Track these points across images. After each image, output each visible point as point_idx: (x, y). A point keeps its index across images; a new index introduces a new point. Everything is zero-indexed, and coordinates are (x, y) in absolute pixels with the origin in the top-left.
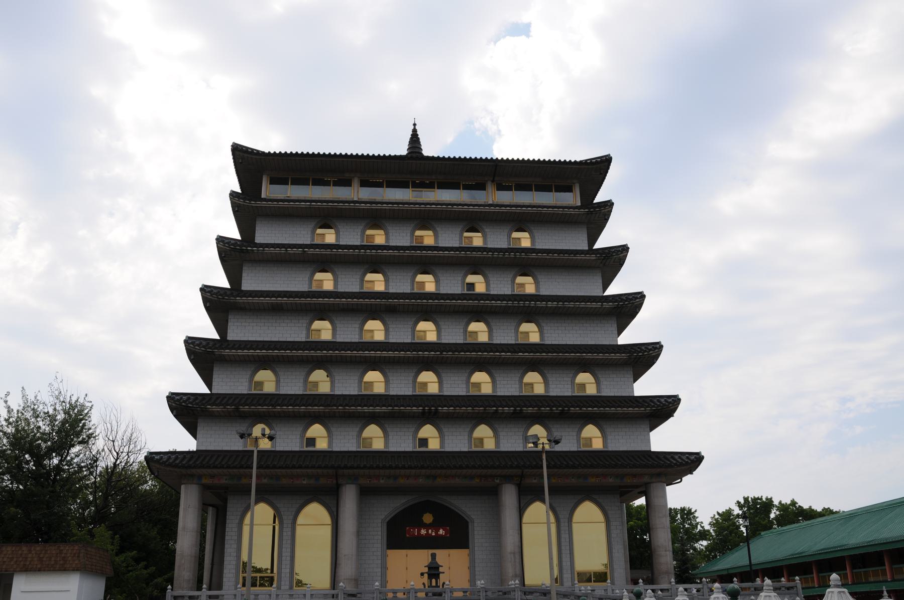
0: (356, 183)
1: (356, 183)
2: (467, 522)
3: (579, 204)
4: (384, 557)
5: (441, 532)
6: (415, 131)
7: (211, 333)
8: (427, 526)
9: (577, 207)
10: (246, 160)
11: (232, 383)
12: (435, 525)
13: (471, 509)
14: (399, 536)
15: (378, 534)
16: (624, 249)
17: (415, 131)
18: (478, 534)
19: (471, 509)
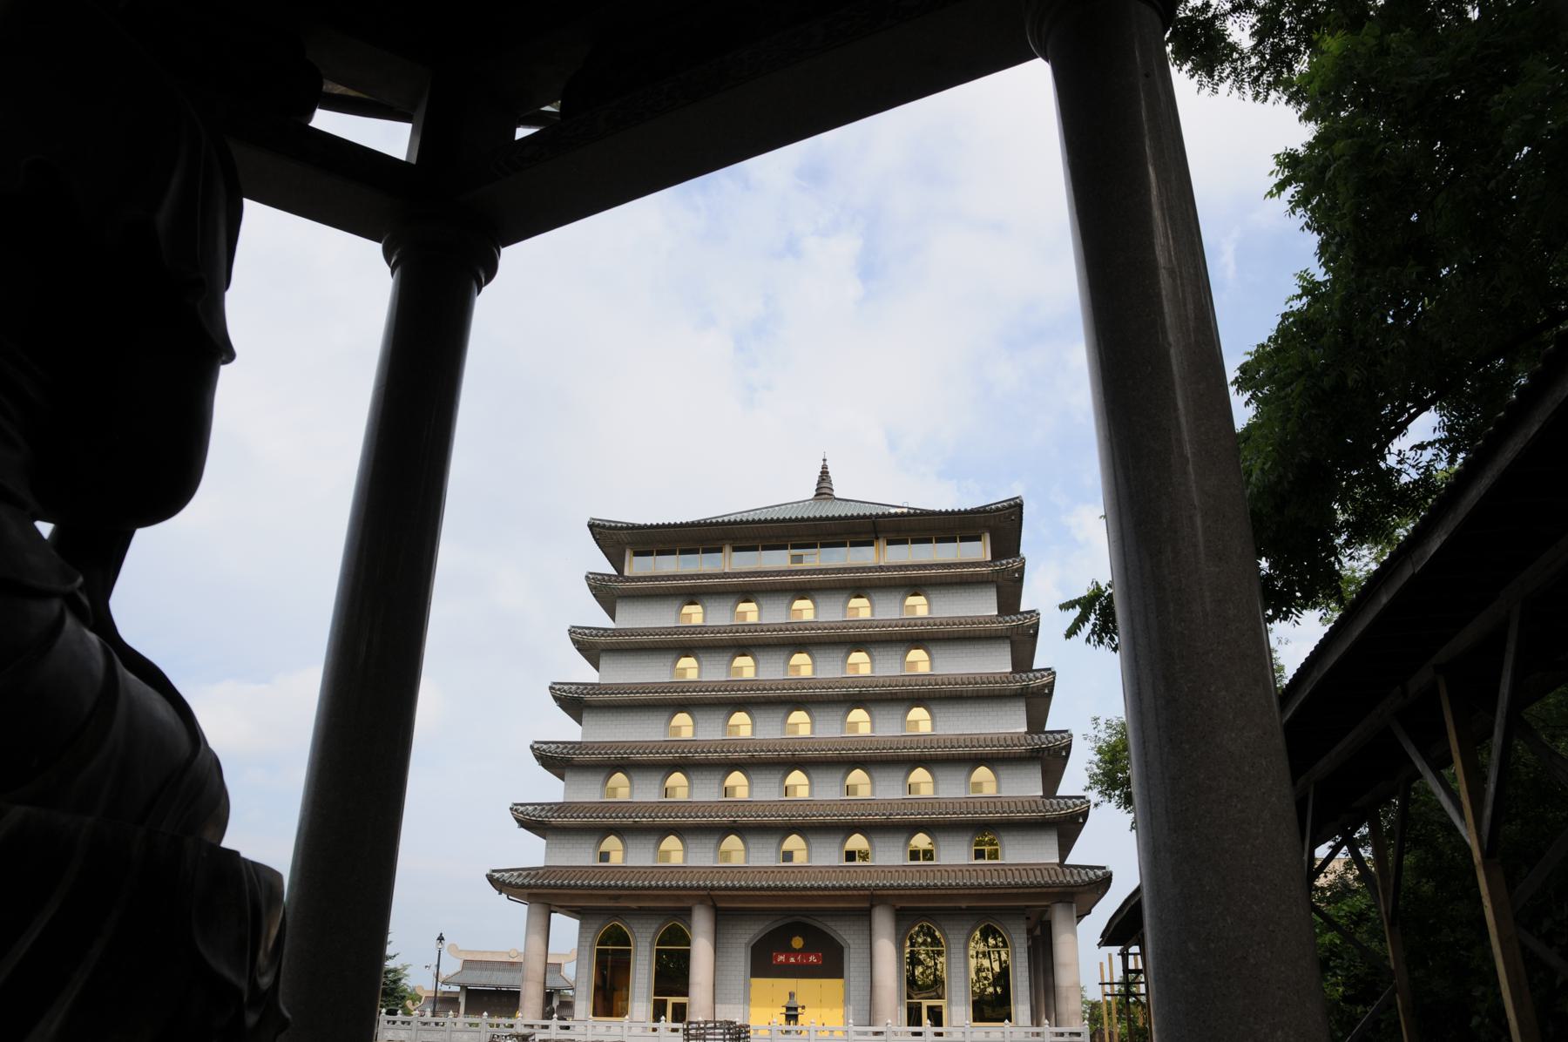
0: (727, 549)
1: (727, 549)
2: (842, 949)
3: (989, 558)
4: (747, 987)
5: (812, 959)
6: (824, 475)
7: (608, 568)
8: (795, 952)
9: (985, 564)
10: (614, 539)
11: (588, 791)
12: (805, 950)
13: (847, 935)
14: (762, 965)
15: (740, 960)
16: (593, 527)
17: (824, 475)
18: (853, 962)
19: (847, 935)
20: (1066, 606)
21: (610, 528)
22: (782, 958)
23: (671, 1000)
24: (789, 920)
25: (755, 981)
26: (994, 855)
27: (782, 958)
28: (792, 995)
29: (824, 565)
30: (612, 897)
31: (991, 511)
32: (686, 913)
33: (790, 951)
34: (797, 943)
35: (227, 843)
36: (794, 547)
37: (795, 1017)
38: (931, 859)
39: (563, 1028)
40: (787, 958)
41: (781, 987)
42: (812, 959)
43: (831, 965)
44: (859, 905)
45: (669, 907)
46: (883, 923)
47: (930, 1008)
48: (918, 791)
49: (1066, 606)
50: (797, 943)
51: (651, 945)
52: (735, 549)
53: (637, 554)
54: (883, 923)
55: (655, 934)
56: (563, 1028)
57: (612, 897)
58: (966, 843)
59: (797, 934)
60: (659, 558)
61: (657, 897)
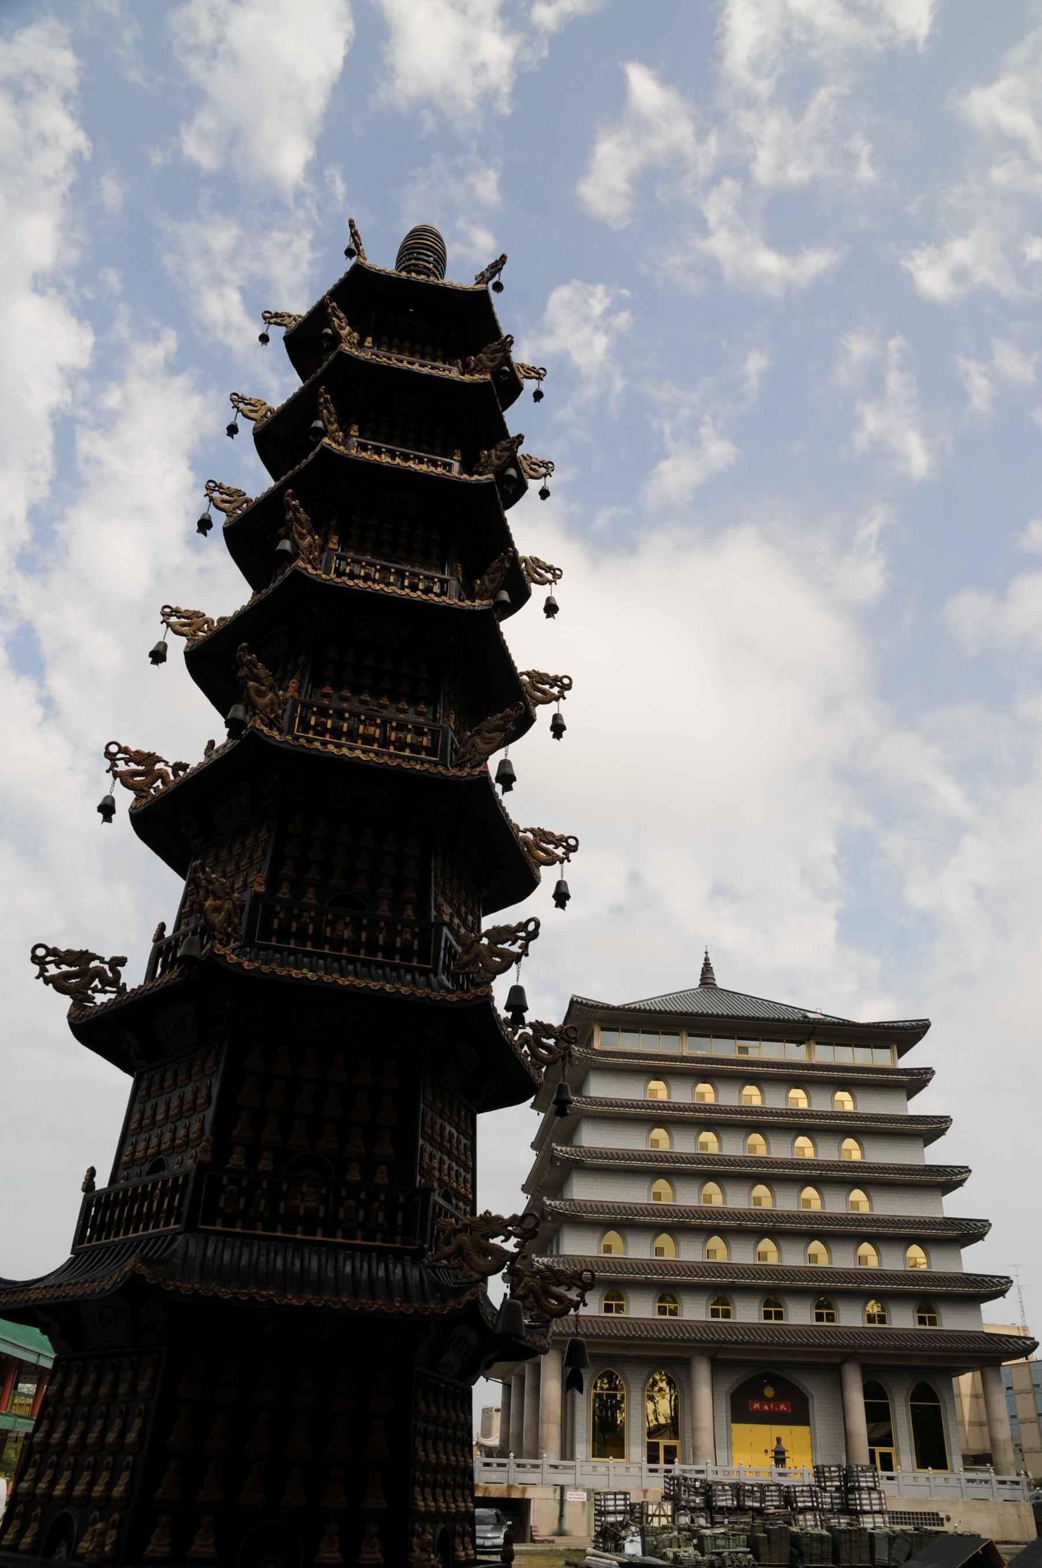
1: (684, 1035)
4: (729, 1431)
5: (782, 1407)
8: (768, 1401)
12: (777, 1399)
17: (707, 969)
18: (819, 1409)
21: (592, 1006)
22: (757, 1406)
25: (737, 1428)
26: (673, 1313)
28: (779, 1440)
29: (700, 1053)
31: (883, 1027)
33: (763, 1399)
34: (769, 1392)
36: (740, 1038)
38: (676, 1314)
39: (780, 1474)
40: (762, 1406)
41: (765, 1434)
42: (782, 1407)
44: (828, 1358)
46: (702, 1373)
47: (666, 1448)
48: (766, 1259)
50: (769, 1392)
52: (690, 1035)
53: (603, 1029)
56: (780, 1474)
58: (651, 1300)
61: (821, 1354)
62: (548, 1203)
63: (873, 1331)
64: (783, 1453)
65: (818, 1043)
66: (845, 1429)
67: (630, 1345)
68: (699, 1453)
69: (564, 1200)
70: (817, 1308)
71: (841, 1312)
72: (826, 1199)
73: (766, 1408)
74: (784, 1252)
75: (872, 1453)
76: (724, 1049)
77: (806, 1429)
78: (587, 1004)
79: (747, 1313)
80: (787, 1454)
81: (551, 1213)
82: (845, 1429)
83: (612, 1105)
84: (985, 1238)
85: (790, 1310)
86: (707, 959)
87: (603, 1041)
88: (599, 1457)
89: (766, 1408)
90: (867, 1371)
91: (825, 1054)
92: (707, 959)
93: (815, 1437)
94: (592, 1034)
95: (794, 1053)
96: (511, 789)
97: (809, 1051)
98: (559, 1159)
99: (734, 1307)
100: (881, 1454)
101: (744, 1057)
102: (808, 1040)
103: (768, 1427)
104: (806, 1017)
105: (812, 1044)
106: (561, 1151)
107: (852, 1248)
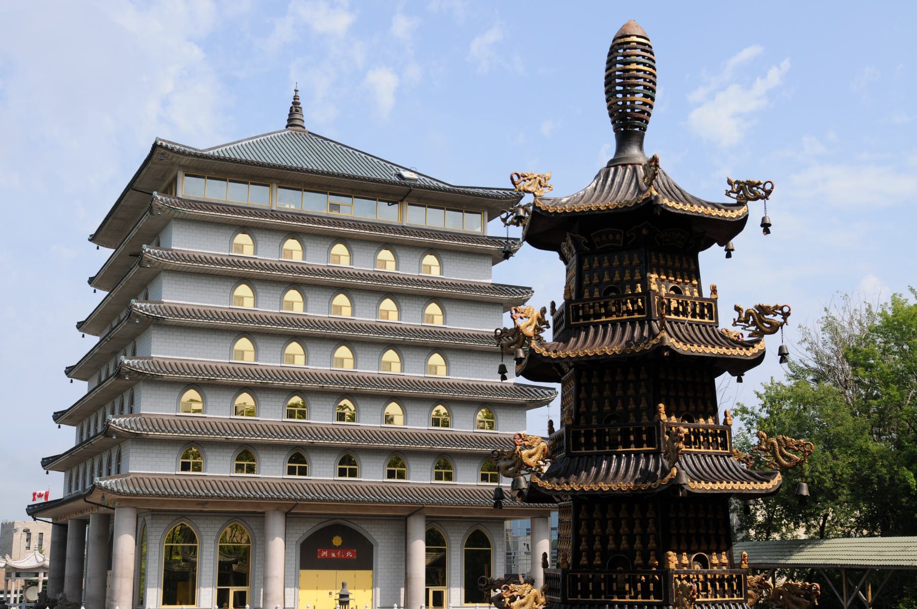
1: (275, 186)
2: (372, 546)
5: (349, 554)
8: (336, 549)
18: (382, 555)
20: (738, 404)
22: (325, 553)
23: (232, 590)
24: (331, 523)
27: (325, 553)
30: (199, 503)
32: (260, 516)
33: (330, 547)
35: (75, 428)
37: (341, 596)
38: (199, 470)
40: (329, 554)
42: (349, 554)
43: (362, 559)
44: (398, 516)
45: (245, 515)
46: (276, 524)
49: (738, 404)
50: (337, 541)
51: (216, 542)
54: (276, 524)
55: (217, 536)
57: (199, 503)
59: (336, 539)
60: (208, 181)
62: (126, 362)
63: (439, 487)
64: (347, 596)
65: (410, 204)
66: (406, 574)
67: (207, 503)
68: (269, 599)
69: (140, 358)
70: (389, 466)
71: (412, 470)
72: (406, 363)
73: (333, 555)
74: (409, 416)
75: (427, 591)
76: (315, 204)
77: (369, 573)
78: (172, 150)
79: (323, 473)
80: (350, 597)
81: (128, 373)
82: (406, 574)
83: (196, 261)
84: (551, 404)
85: (364, 468)
86: (296, 103)
87: (191, 188)
88: (168, 604)
89: (333, 555)
90: (429, 520)
91: (417, 217)
92: (296, 103)
93: (376, 580)
94: (175, 179)
95: (387, 213)
96: (762, 226)
97: (401, 211)
98: (138, 316)
99: (311, 464)
100: (434, 592)
101: (335, 214)
102: (402, 201)
103: (334, 572)
104: (400, 176)
105: (405, 204)
106: (141, 308)
107: (428, 409)
